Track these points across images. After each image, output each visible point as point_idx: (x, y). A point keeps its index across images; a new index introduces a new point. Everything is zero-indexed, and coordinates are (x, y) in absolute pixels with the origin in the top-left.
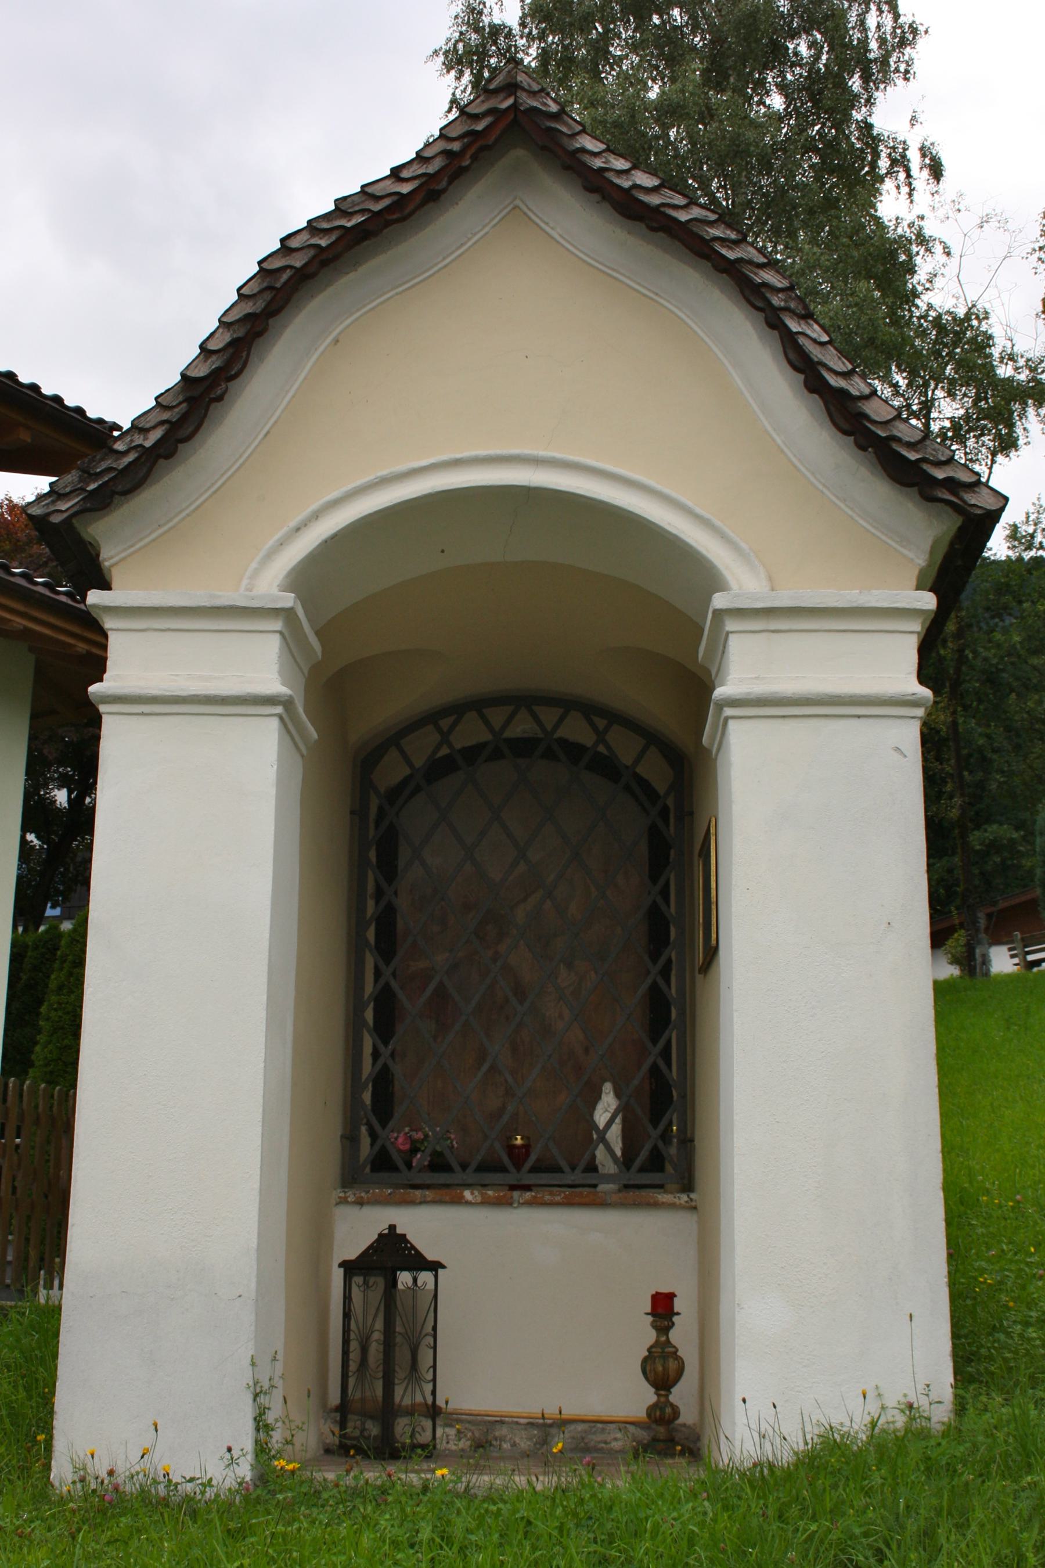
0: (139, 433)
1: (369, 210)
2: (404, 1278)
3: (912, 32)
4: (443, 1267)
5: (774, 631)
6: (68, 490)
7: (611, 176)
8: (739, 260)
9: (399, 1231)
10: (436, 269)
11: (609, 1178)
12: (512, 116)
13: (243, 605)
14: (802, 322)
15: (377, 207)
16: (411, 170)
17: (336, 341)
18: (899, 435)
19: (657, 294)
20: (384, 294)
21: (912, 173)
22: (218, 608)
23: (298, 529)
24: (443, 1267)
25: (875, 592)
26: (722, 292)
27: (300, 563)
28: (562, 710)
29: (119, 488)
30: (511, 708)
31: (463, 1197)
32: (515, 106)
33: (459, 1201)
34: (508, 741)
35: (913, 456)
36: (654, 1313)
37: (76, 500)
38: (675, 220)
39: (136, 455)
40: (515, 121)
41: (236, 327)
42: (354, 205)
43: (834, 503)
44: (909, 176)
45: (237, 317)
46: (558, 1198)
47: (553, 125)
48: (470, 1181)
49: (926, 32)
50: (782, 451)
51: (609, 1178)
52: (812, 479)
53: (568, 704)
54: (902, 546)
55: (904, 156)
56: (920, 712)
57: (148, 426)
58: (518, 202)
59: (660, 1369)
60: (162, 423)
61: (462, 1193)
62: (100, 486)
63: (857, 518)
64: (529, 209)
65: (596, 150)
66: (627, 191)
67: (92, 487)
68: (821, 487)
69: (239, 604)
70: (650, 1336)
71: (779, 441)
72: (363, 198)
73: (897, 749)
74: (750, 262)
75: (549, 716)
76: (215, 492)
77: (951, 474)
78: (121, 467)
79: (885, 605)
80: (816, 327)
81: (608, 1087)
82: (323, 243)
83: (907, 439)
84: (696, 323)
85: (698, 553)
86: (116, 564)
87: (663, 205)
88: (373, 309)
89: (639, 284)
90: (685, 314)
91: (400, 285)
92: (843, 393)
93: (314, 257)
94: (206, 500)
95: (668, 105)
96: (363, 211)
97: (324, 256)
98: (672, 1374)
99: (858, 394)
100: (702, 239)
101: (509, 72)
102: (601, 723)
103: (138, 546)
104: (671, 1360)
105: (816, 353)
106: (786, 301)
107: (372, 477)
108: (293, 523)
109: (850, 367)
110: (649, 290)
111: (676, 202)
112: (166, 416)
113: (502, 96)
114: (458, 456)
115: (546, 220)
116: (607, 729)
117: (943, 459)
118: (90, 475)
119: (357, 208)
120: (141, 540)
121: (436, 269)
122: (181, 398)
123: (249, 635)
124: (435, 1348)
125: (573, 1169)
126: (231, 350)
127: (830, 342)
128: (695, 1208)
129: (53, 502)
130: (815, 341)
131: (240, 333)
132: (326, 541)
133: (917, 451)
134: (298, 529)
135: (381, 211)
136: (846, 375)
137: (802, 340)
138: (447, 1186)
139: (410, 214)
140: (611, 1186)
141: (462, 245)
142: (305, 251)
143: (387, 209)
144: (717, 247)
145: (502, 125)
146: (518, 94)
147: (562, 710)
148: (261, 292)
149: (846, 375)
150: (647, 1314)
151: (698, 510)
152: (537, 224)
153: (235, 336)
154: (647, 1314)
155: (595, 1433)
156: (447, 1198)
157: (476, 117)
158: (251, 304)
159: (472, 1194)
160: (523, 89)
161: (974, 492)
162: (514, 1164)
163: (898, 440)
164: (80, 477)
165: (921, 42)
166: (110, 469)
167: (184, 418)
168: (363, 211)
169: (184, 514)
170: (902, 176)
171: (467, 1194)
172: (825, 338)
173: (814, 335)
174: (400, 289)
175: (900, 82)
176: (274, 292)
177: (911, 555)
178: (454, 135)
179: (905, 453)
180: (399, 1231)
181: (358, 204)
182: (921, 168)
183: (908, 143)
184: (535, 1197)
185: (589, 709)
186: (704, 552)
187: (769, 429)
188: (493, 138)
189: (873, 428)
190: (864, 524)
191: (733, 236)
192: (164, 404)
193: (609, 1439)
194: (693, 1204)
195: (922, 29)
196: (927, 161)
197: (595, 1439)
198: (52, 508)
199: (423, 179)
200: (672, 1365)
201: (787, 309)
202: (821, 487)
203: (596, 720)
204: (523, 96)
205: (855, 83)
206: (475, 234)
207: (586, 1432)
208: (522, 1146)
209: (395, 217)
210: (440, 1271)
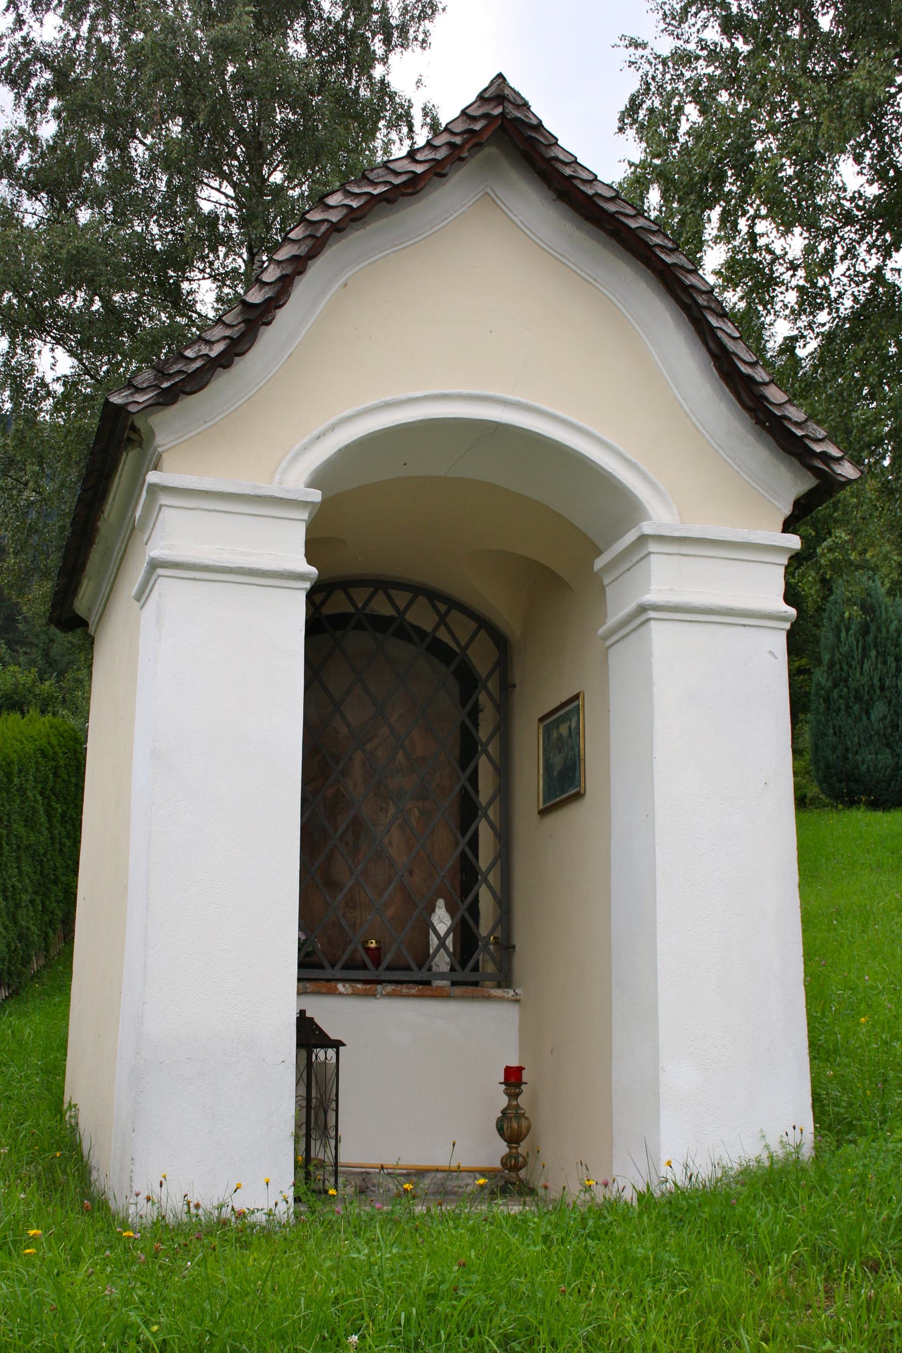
0: (206, 344)
1: (390, 183)
2: (321, 1053)
3: (431, 8)
4: (344, 1045)
5: (683, 555)
6: (145, 385)
7: (577, 183)
8: (675, 265)
9: (308, 1015)
10: (425, 235)
11: (442, 976)
12: (500, 122)
13: (280, 496)
14: (720, 320)
15: (397, 181)
16: (424, 154)
17: (345, 285)
18: (789, 415)
19: (596, 280)
20: (385, 250)
21: (414, 129)
22: (259, 496)
23: (318, 437)
24: (344, 1045)
25: (760, 532)
26: (647, 285)
27: (320, 465)
28: (411, 595)
29: (188, 389)
30: (371, 589)
31: (337, 989)
32: (502, 114)
33: (334, 993)
34: (367, 615)
35: (799, 433)
36: (507, 1082)
37: (151, 395)
38: (627, 227)
39: (203, 363)
40: (501, 127)
41: (284, 265)
42: (379, 177)
43: (725, 460)
44: (411, 130)
45: (286, 257)
46: (413, 991)
47: (533, 135)
48: (338, 976)
49: (444, 10)
50: (687, 416)
51: (442, 976)
52: (710, 439)
53: (417, 590)
54: (774, 498)
55: (408, 114)
56: (788, 626)
57: (213, 339)
58: (488, 190)
59: (516, 1126)
60: (225, 338)
61: (336, 986)
62: (172, 385)
63: (742, 473)
64: (498, 197)
65: (567, 161)
66: (589, 198)
67: (165, 385)
68: (716, 446)
69: (277, 495)
70: (504, 1101)
71: (686, 407)
72: (386, 172)
73: (771, 652)
74: (682, 267)
75: (403, 600)
76: (249, 399)
77: (825, 449)
78: (190, 371)
79: (767, 542)
80: (730, 324)
81: (441, 903)
82: (355, 204)
83: (796, 419)
84: (625, 307)
85: (626, 488)
86: (167, 450)
87: (618, 212)
88: (374, 262)
89: (582, 270)
90: (617, 299)
91: (397, 245)
92: (750, 378)
93: (346, 215)
94: (241, 405)
95: (223, 40)
96: (386, 183)
97: (353, 216)
98: (524, 1130)
99: (761, 380)
100: (646, 244)
101: (499, 85)
102: (443, 608)
103: (185, 438)
104: (523, 1120)
105: (731, 345)
106: (708, 302)
107: (378, 401)
108: (315, 433)
109: (755, 359)
110: (589, 276)
111: (628, 212)
112: (228, 332)
113: (493, 104)
114: (446, 392)
115: (511, 208)
116: (448, 612)
117: (820, 437)
118: (164, 375)
119: (381, 180)
120: (190, 432)
121: (425, 235)
122: (240, 319)
123: (747, 564)
124: (337, 1111)
125: (420, 969)
126: (280, 284)
127: (740, 338)
128: (518, 1001)
129: (132, 394)
130: (729, 336)
131: (288, 270)
132: (341, 450)
133: (802, 429)
134: (318, 437)
135: (398, 185)
136: (752, 365)
137: (720, 334)
138: (328, 980)
139: (421, 190)
140: (445, 982)
141: (446, 219)
142: (339, 209)
143: (404, 184)
144: (658, 251)
145: (492, 128)
146: (505, 104)
147: (411, 595)
148: (304, 238)
149: (752, 365)
150: (501, 1083)
151: (628, 456)
152: (503, 211)
153: (284, 273)
154: (501, 1083)
155: (451, 1180)
156: (324, 990)
157: (473, 119)
158: (296, 247)
159: (344, 986)
160: (510, 101)
161: (840, 464)
162: (374, 964)
163: (789, 419)
164: (155, 375)
165: (439, 17)
166: (180, 372)
167: (242, 336)
168: (386, 183)
169: (224, 414)
170: (405, 130)
171: (340, 987)
172: (737, 335)
173: (729, 331)
174: (397, 248)
175: (418, 49)
176: (314, 240)
177: (780, 506)
178: (457, 130)
179: (793, 429)
180: (308, 1015)
181: (382, 176)
182: (422, 126)
183: (413, 101)
184: (394, 990)
185: (433, 596)
186: (632, 489)
187: (679, 397)
188: (486, 137)
189: (771, 408)
190: (748, 479)
191: (670, 245)
192: (227, 322)
193: (462, 1184)
194: (518, 997)
195: (440, 6)
196: (428, 120)
197: (450, 1184)
198: (131, 399)
199: (433, 164)
200: (524, 1123)
201: (709, 308)
202: (716, 446)
203: (439, 604)
204: (510, 107)
205: (378, 46)
206: (455, 211)
207: (444, 1178)
208: (376, 949)
209: (409, 191)
210: (341, 1048)
